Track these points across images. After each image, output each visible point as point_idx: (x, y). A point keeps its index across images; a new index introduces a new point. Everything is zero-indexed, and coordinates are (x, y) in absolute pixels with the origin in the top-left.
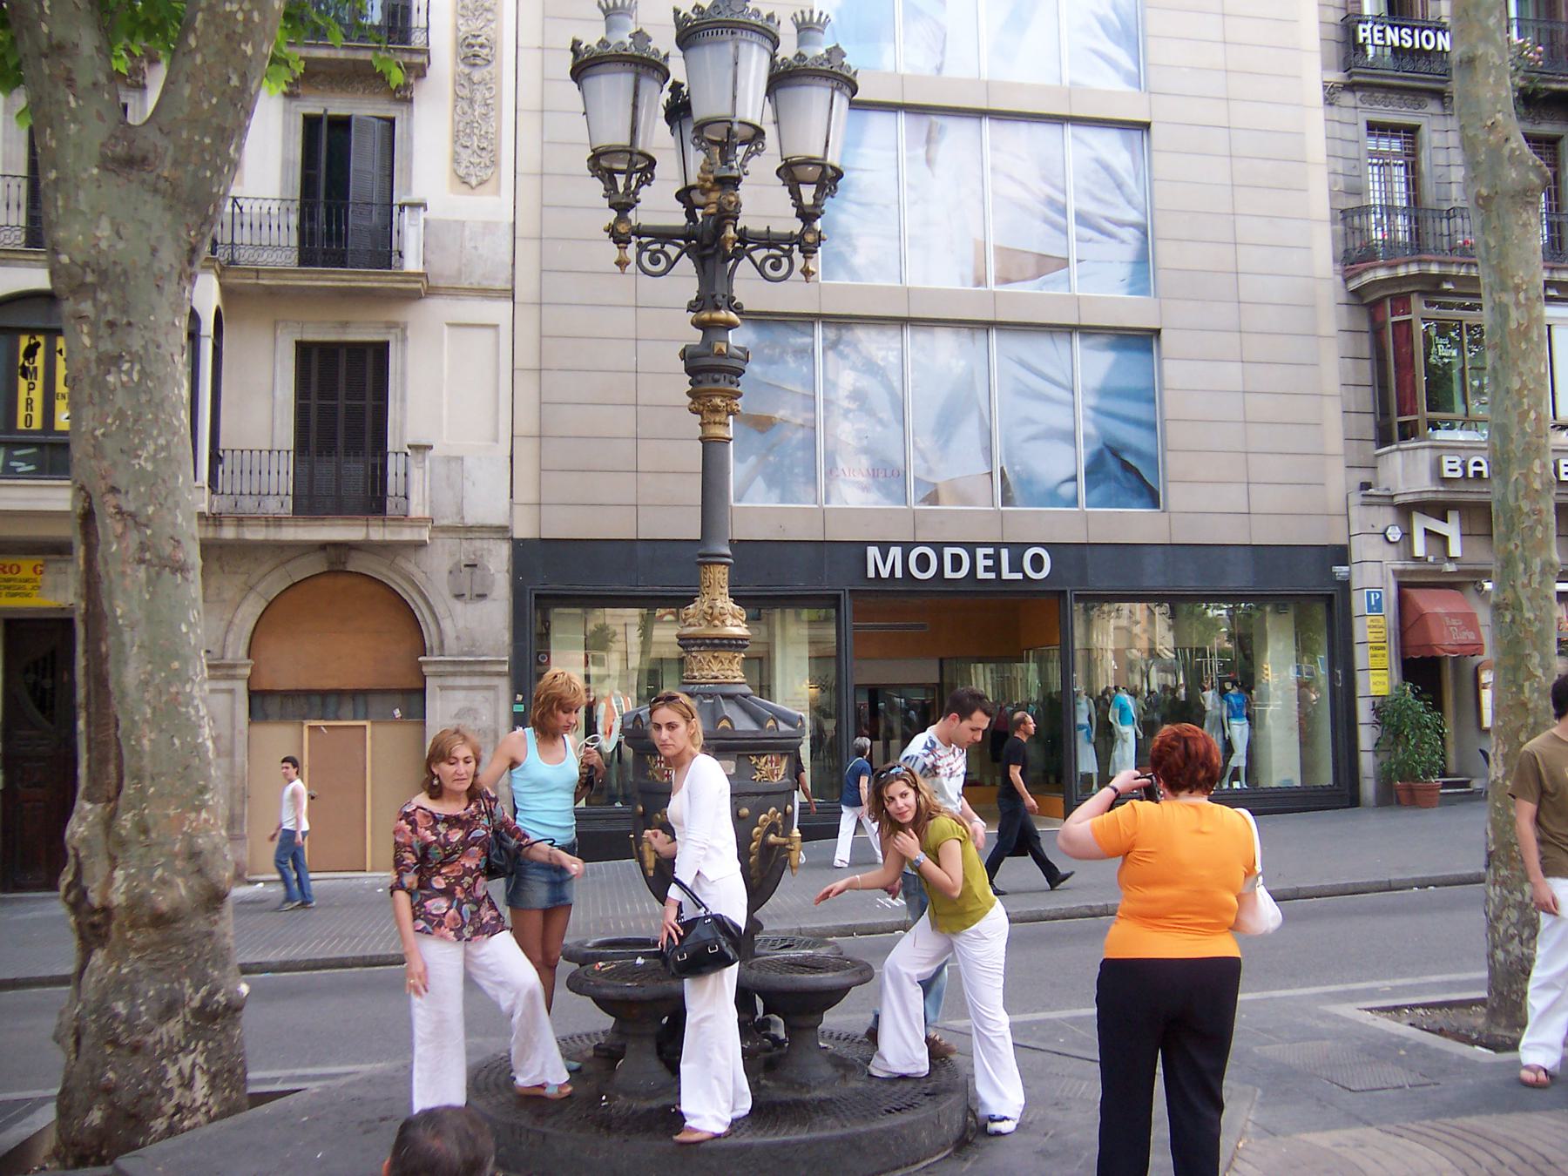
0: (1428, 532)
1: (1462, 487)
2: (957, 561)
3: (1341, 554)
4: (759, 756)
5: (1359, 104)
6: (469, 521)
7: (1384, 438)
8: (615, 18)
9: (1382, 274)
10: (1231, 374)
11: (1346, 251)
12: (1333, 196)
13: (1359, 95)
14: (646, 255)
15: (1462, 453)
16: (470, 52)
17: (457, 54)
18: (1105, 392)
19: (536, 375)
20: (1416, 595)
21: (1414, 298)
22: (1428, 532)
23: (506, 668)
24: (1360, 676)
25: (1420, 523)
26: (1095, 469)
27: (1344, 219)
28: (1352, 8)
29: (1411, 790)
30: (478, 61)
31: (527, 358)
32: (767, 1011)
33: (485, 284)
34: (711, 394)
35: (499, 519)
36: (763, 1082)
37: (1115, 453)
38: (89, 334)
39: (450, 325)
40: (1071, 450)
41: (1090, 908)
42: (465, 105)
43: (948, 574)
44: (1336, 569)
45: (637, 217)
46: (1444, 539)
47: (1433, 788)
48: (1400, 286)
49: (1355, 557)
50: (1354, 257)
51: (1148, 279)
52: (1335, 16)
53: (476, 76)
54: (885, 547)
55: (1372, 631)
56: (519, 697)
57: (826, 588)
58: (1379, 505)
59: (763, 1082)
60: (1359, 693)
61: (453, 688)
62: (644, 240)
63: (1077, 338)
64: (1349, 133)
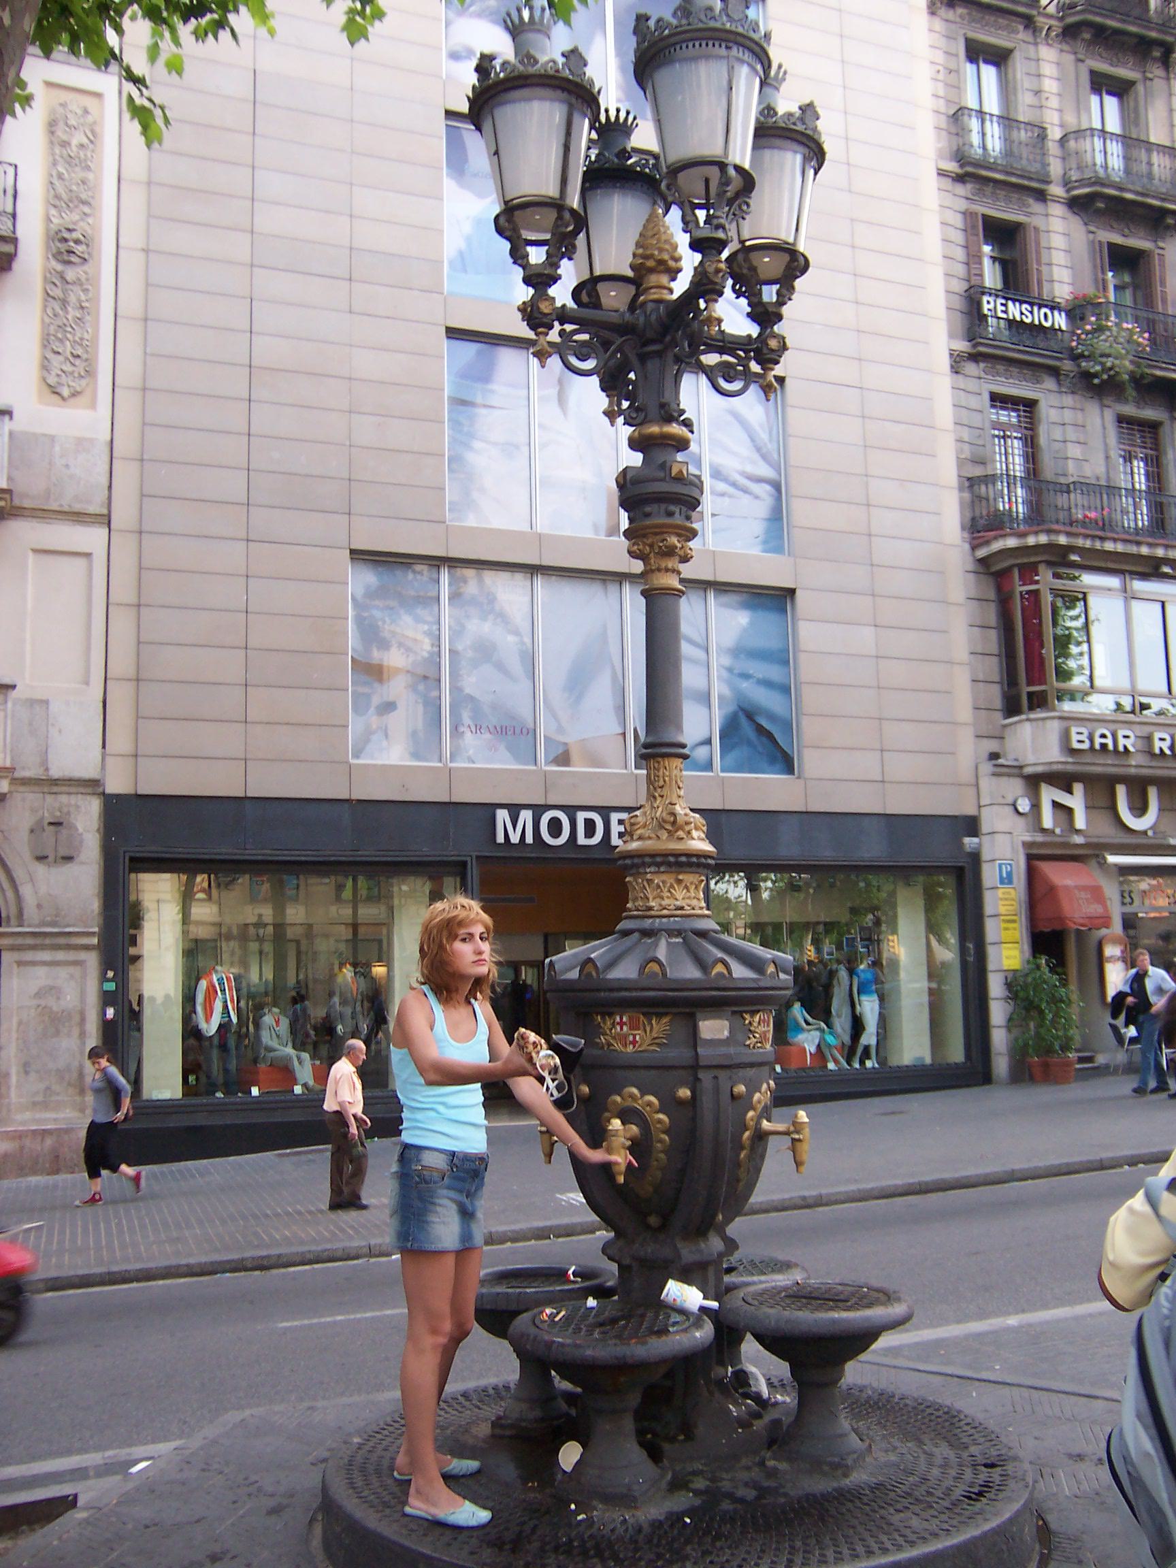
0: (1056, 805)
1: (1088, 758)
2: (590, 827)
3: (971, 825)
4: (753, 1013)
5: (983, 375)
6: (55, 773)
7: (1012, 707)
8: (531, 36)
9: (1012, 542)
10: (865, 638)
11: (973, 519)
12: (961, 463)
13: (982, 365)
15: (1088, 724)
16: (63, 247)
17: (48, 248)
18: (739, 651)
19: (134, 611)
20: (1047, 868)
21: (1042, 568)
22: (1056, 805)
23: (95, 941)
24: (991, 951)
25: (1049, 794)
26: (730, 732)
27: (971, 486)
28: (975, 280)
29: (1046, 1066)
30: (73, 259)
31: (124, 591)
33: (78, 507)
34: (662, 530)
35: (89, 770)
36: (771, 1463)
37: (750, 716)
39: (35, 551)
40: (705, 711)
41: (804, 1198)
42: (57, 306)
43: (582, 840)
44: (967, 840)
46: (1070, 811)
47: (1068, 1064)
48: (1029, 555)
49: (985, 827)
50: (982, 524)
51: (782, 538)
52: (960, 287)
53: (70, 274)
54: (514, 810)
55: (1003, 905)
56: (110, 974)
57: (451, 854)
58: (1009, 775)
59: (771, 1463)
60: (991, 965)
61: (34, 963)
62: (569, 327)
63: (711, 595)
64: (974, 402)
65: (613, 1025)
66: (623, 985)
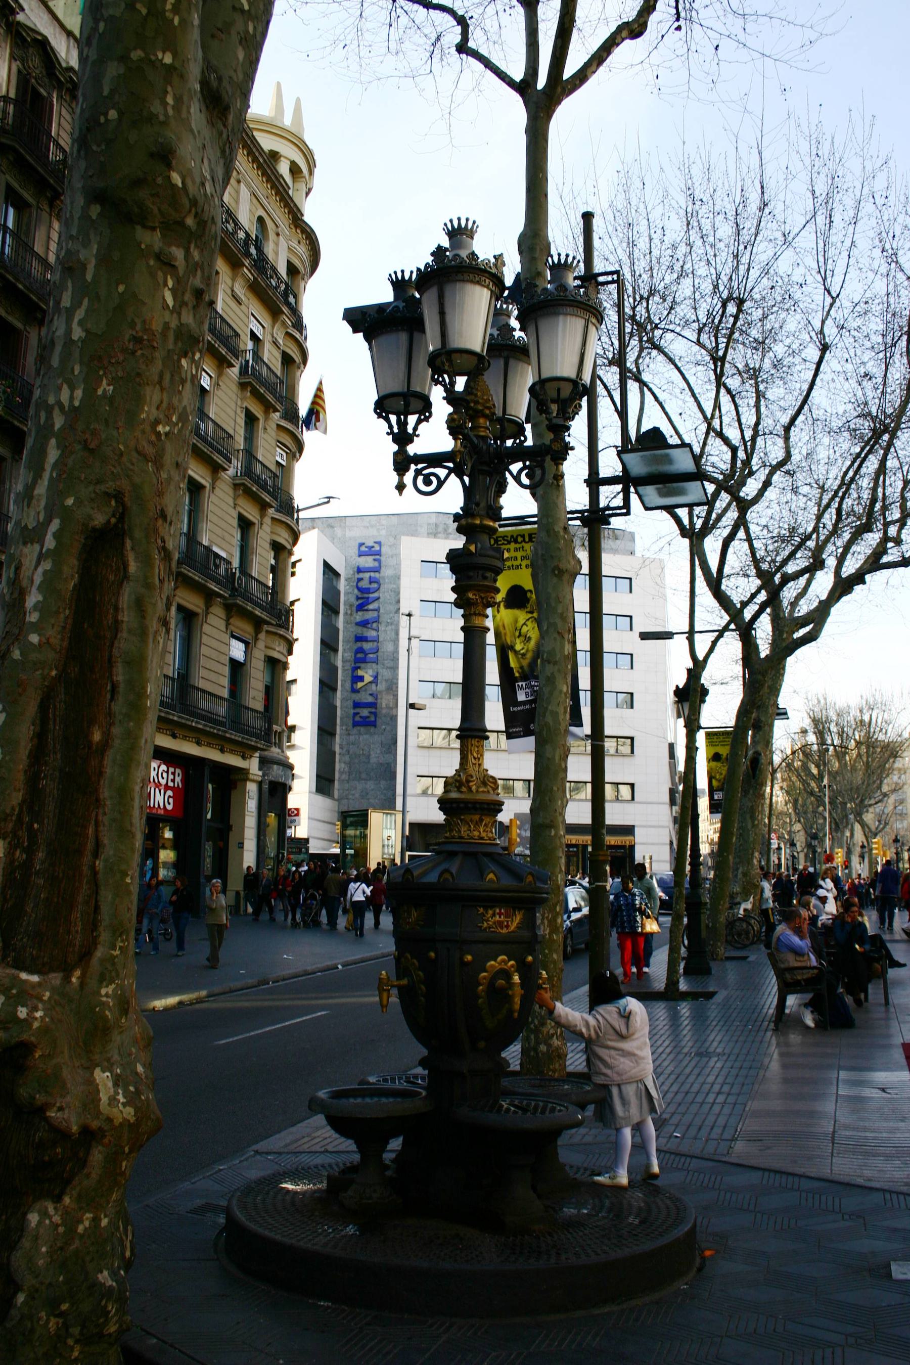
14: (420, 478)
32: (495, 960)
38: (173, 291)
45: (412, 449)
62: (420, 466)
65: (494, 915)
66: (430, 886)
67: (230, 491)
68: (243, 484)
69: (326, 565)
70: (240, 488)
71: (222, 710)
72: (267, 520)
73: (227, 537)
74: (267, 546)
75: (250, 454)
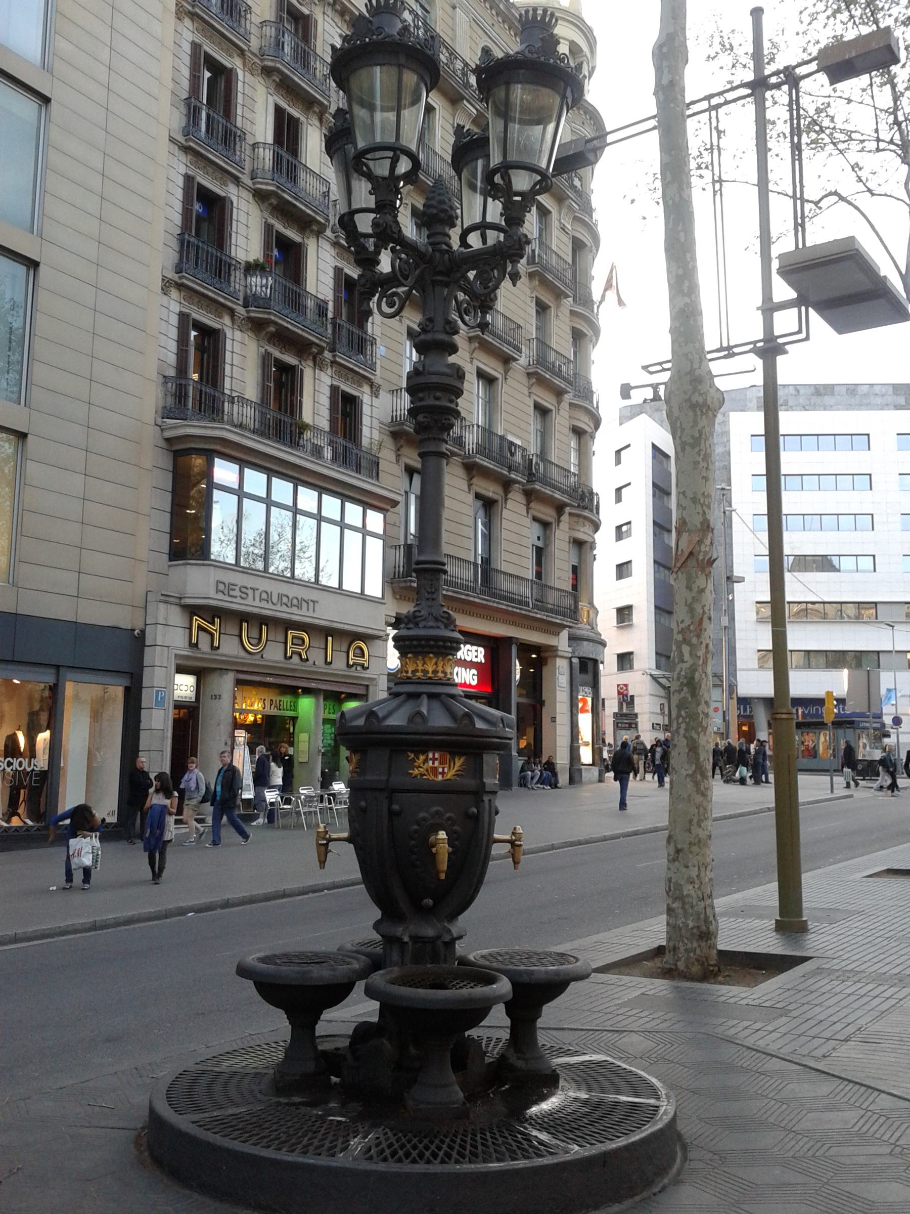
65: (426, 761)
66: (395, 730)
67: (524, 380)
68: (536, 373)
69: (654, 446)
70: (535, 378)
71: (526, 591)
72: (565, 405)
73: (523, 425)
74: (566, 431)
75: (543, 344)
